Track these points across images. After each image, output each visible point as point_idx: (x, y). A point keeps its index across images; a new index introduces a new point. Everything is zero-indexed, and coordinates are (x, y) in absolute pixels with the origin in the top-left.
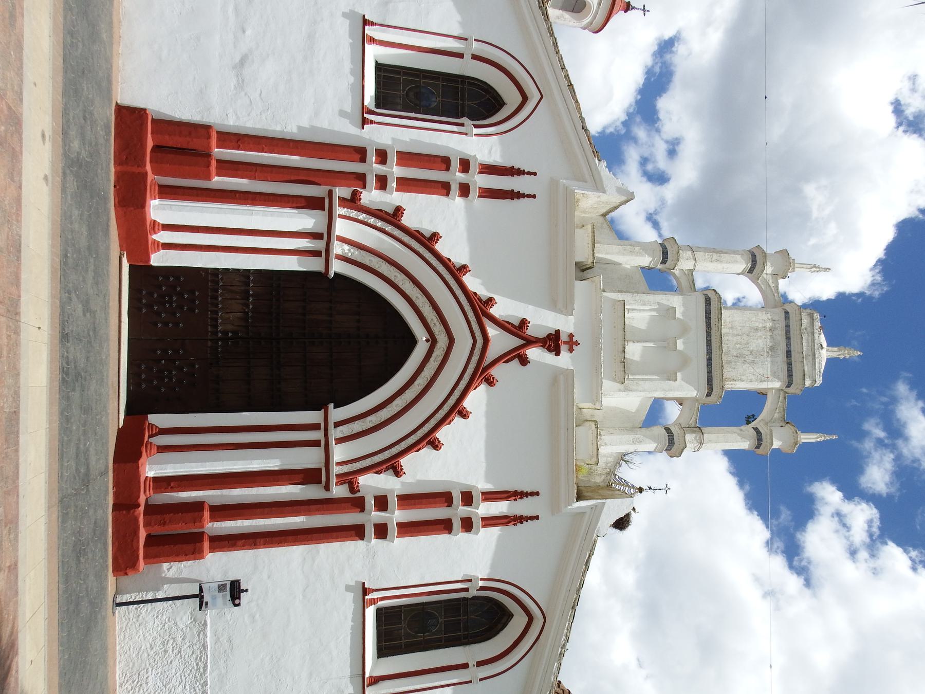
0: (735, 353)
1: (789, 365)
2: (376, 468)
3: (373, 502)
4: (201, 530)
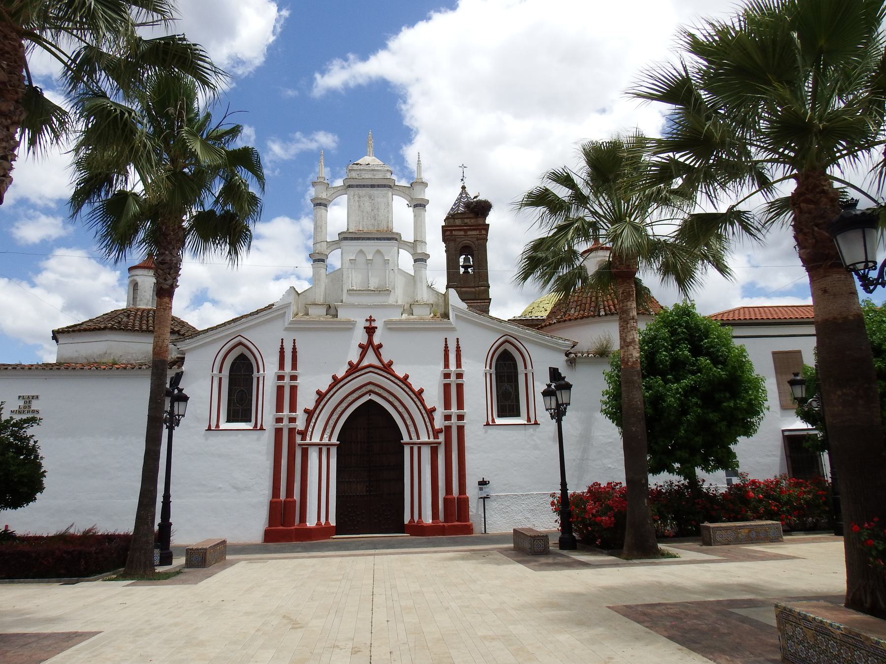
0: (373, 221)
1: (379, 186)
2: (432, 420)
3: (447, 422)
4: (456, 499)
